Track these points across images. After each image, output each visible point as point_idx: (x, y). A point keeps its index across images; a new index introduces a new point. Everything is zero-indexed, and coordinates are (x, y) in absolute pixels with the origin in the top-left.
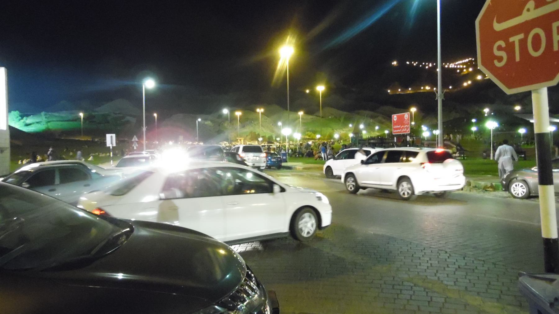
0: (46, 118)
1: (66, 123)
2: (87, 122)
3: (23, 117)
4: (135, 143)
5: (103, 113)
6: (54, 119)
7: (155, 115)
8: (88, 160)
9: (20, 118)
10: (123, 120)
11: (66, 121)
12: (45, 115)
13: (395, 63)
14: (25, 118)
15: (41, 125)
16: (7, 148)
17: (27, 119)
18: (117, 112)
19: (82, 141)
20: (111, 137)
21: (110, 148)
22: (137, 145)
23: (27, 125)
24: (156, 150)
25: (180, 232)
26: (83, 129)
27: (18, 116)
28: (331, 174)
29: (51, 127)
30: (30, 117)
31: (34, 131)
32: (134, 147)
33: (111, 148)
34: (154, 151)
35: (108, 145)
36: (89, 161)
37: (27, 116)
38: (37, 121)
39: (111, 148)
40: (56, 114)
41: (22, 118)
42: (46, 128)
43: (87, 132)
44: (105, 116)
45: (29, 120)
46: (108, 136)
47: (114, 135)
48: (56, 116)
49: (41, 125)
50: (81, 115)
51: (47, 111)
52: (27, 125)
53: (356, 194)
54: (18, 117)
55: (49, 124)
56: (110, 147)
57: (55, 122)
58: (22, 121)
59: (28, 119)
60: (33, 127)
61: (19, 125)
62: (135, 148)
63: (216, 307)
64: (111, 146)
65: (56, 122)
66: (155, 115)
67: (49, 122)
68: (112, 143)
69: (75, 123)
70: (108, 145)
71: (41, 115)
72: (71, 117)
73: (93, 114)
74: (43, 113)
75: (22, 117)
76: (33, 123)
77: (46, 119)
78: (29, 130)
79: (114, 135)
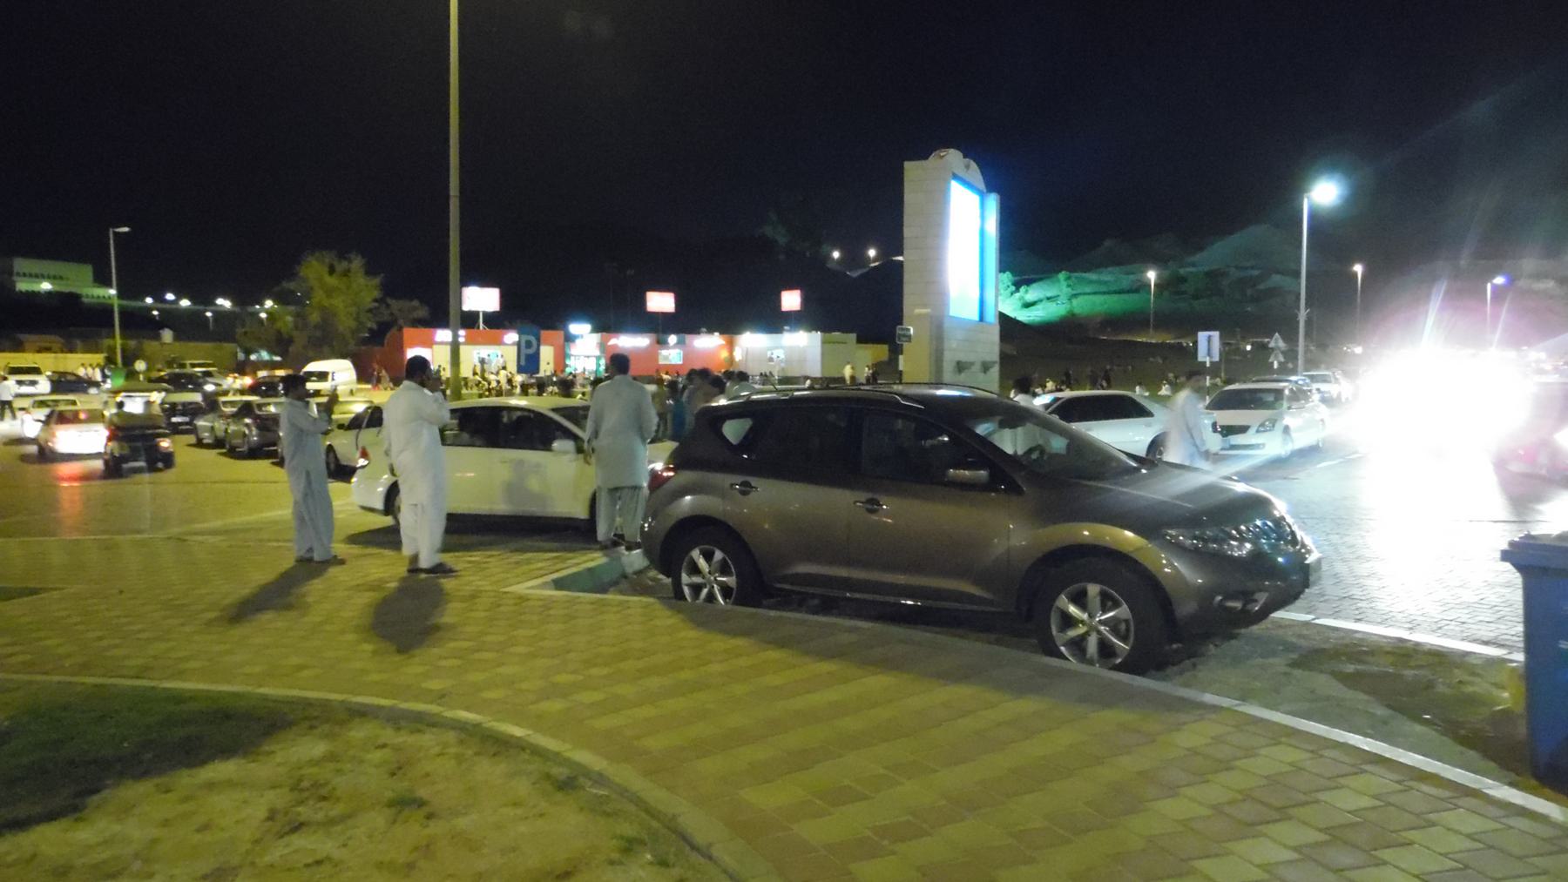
0: (1069, 286)
1: (1115, 297)
2: (1166, 293)
3: (1021, 287)
4: (1275, 352)
5: (1206, 269)
6: (1088, 290)
7: (1358, 269)
8: (1159, 393)
9: (1013, 288)
10: (1262, 287)
11: (1116, 292)
12: (1069, 278)
13: (836, 255)
14: (1023, 289)
15: (1057, 304)
16: (994, 363)
17: (1027, 292)
18: (1249, 264)
19: (1151, 344)
20: (1209, 338)
21: (1205, 366)
22: (1282, 359)
23: (1027, 305)
24: (1339, 375)
25: (708, 471)
26: (1155, 312)
27: (1010, 284)
28: (581, 412)
29: (1077, 310)
30: (1034, 285)
31: (1043, 319)
32: (1272, 363)
33: (1208, 365)
34: (1329, 375)
35: (1200, 359)
36: (1160, 396)
37: (1028, 282)
38: (1049, 295)
39: (1208, 365)
40: (1093, 276)
41: (1017, 290)
42: (1068, 312)
43: (1164, 321)
44: (1213, 275)
45: (1031, 293)
46: (1202, 336)
47: (1216, 335)
48: (1091, 282)
49: (1057, 304)
50: (1152, 275)
51: (1072, 270)
52: (1027, 305)
53: (88, 393)
54: (1008, 286)
55: (1075, 302)
56: (1205, 362)
57: (1086, 297)
58: (1017, 295)
59: (1030, 292)
60: (1038, 310)
61: (1012, 308)
62: (1276, 365)
63: (472, 475)
64: (1208, 360)
65: (1091, 297)
66: (1358, 269)
67: (1075, 296)
68: (1209, 354)
69: (1135, 297)
70: (1200, 359)
71: (1059, 281)
72: (1126, 281)
73: (1182, 271)
74: (1062, 276)
75: (1018, 285)
76: (1041, 301)
77: (1069, 289)
78: (1031, 318)
79: (1216, 335)
